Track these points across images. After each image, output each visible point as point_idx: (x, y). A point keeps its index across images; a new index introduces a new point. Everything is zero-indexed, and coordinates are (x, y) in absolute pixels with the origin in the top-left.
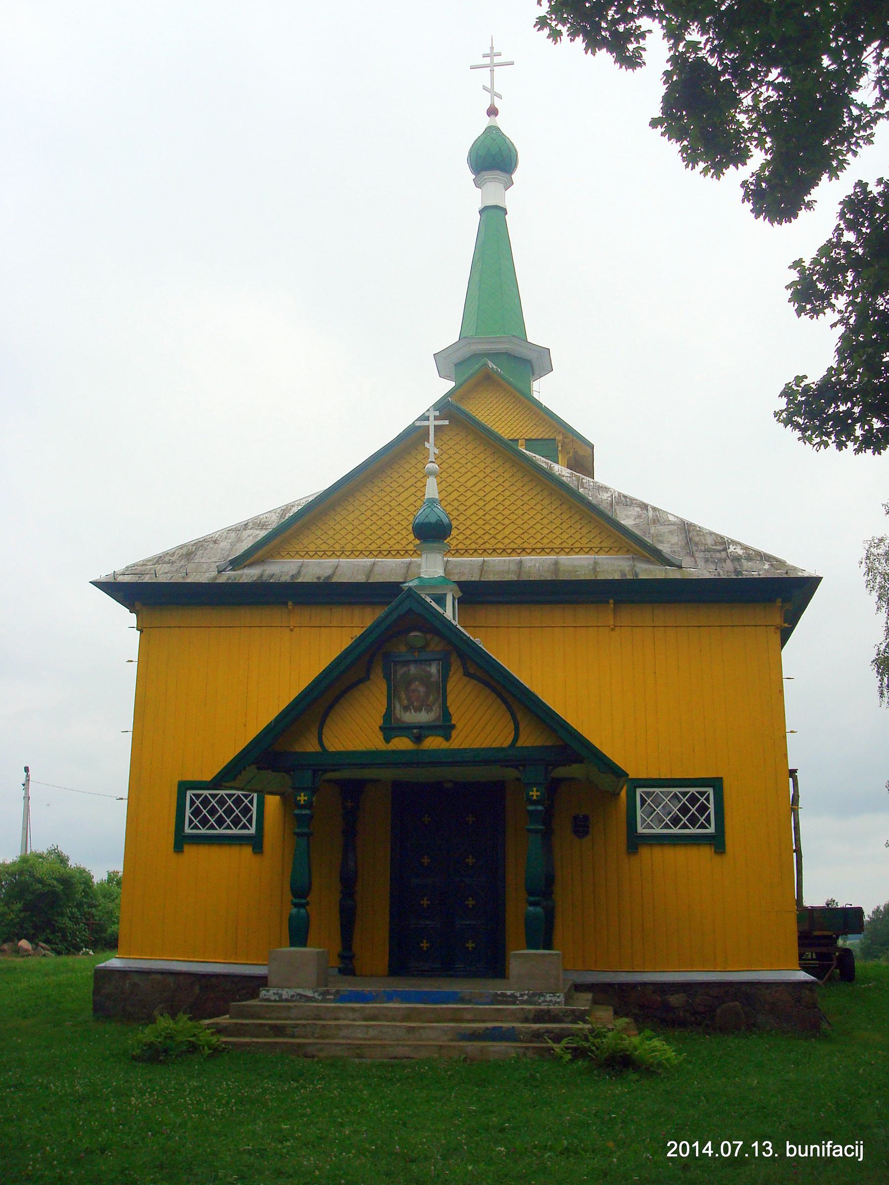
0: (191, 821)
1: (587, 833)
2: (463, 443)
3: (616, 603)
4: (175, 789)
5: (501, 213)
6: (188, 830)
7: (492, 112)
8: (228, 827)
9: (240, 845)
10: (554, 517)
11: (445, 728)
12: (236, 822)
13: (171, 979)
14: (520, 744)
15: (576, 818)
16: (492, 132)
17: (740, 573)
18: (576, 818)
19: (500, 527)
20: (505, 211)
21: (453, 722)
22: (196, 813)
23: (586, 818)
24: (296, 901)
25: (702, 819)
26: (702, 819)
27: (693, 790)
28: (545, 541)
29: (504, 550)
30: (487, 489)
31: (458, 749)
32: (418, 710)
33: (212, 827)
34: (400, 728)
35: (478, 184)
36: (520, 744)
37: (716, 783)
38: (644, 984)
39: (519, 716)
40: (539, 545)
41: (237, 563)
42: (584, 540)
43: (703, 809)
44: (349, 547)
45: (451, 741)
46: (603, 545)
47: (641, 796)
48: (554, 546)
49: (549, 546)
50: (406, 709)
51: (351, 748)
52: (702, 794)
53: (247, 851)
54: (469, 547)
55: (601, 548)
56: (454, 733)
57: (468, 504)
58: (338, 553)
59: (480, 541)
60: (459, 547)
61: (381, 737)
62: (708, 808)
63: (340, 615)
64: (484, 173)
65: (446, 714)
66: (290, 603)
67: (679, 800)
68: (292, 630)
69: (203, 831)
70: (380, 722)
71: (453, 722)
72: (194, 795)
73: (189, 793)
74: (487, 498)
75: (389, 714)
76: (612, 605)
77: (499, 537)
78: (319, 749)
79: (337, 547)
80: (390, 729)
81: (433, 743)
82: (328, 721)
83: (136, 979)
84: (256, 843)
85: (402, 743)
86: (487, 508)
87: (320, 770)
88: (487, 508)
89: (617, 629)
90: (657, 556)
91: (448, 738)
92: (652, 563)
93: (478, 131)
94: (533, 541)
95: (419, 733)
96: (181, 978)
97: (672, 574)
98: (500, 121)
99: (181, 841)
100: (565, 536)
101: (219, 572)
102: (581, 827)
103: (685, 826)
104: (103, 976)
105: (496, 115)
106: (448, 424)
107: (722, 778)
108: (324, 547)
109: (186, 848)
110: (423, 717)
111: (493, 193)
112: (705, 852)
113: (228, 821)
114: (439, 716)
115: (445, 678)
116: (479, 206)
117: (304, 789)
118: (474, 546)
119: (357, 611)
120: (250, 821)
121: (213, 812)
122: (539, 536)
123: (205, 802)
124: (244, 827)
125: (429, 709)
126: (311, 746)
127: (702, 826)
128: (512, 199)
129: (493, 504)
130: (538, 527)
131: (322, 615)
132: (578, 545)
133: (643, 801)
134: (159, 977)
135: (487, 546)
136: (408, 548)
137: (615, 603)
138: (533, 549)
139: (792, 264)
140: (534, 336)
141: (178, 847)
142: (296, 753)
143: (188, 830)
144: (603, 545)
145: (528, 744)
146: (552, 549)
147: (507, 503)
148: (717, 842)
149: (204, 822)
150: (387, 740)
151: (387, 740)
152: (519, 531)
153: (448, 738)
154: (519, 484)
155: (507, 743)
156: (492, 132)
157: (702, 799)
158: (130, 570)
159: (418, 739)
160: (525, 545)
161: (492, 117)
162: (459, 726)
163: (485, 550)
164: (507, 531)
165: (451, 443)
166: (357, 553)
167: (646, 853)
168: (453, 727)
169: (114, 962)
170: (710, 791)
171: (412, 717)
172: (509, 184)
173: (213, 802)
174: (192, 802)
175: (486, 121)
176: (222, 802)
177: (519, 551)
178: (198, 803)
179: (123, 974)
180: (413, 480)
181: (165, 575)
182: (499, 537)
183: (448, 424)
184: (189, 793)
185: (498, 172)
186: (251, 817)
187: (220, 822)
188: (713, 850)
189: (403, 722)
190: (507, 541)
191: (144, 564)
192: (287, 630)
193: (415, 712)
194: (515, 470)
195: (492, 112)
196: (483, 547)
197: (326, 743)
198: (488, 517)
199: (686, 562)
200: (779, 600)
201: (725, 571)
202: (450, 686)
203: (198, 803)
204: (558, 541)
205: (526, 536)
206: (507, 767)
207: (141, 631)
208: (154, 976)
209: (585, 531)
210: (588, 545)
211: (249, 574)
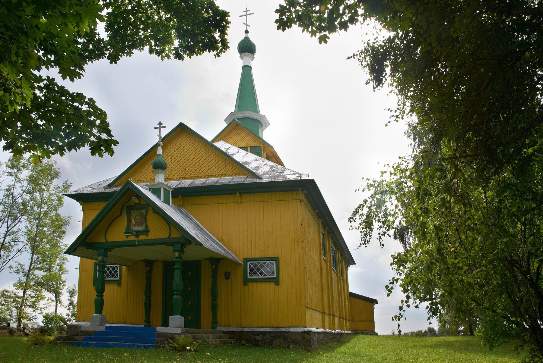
1: (229, 278)
2: (188, 138)
3: (240, 193)
9: (114, 283)
10: (219, 163)
11: (146, 232)
14: (172, 236)
15: (226, 273)
16: (247, 38)
18: (226, 273)
19: (200, 168)
23: (229, 273)
28: (216, 172)
30: (197, 154)
31: (151, 239)
32: (138, 226)
35: (241, 57)
36: (172, 236)
39: (172, 226)
41: (110, 186)
42: (231, 171)
44: (149, 179)
46: (237, 172)
47: (249, 264)
48: (220, 174)
49: (217, 174)
51: (115, 240)
53: (116, 285)
54: (190, 176)
55: (236, 174)
56: (149, 234)
57: (189, 160)
59: (193, 174)
60: (186, 176)
65: (147, 227)
71: (149, 229)
74: (196, 158)
75: (128, 227)
77: (200, 172)
80: (128, 232)
81: (142, 237)
82: (108, 231)
84: (119, 283)
85: (132, 238)
89: (242, 203)
91: (147, 236)
92: (254, 178)
93: (242, 38)
97: (257, 180)
102: (227, 276)
106: (93, 116)
110: (140, 228)
111: (247, 61)
112: (272, 285)
115: (147, 214)
118: (191, 176)
121: (110, 272)
124: (115, 277)
125: (142, 225)
126: (102, 240)
128: (254, 64)
133: (273, 273)
135: (196, 175)
136: (169, 178)
138: (212, 176)
142: (100, 243)
144: (237, 172)
145: (174, 236)
148: (276, 281)
150: (127, 237)
151: (127, 237)
153: (147, 236)
156: (247, 38)
159: (137, 236)
160: (209, 174)
161: (247, 33)
162: (151, 231)
163: (195, 177)
165: (182, 140)
167: (250, 285)
168: (149, 231)
172: (253, 59)
175: (244, 35)
177: (207, 177)
180: (171, 153)
182: (200, 172)
183: (93, 116)
190: (203, 173)
196: (194, 176)
204: (221, 172)
206: (169, 245)
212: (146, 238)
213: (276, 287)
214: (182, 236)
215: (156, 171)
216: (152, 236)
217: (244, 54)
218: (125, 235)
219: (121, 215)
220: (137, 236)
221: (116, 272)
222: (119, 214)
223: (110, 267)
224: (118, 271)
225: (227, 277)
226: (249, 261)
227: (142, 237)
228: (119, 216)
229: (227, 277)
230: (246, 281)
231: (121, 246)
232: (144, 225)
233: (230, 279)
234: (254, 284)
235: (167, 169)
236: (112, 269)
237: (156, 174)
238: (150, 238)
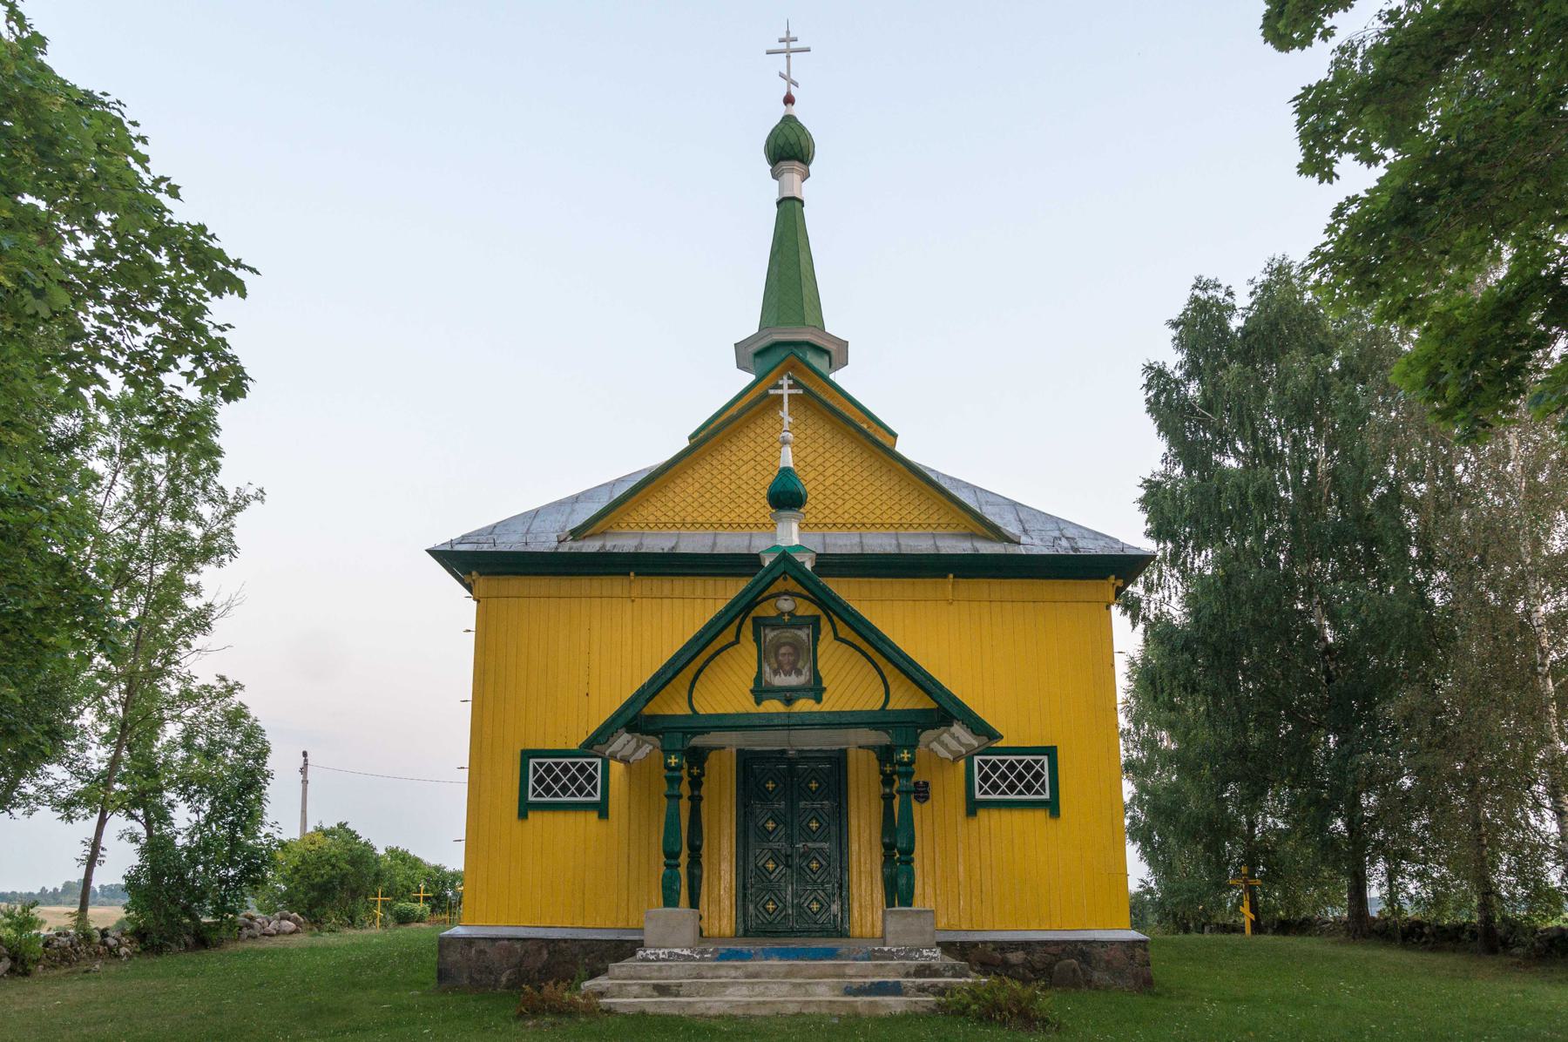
0: (534, 790)
1: (927, 798)
4: (518, 759)
5: (797, 204)
6: (531, 798)
7: (789, 100)
8: (573, 795)
11: (816, 689)
12: (580, 790)
13: (518, 946)
14: (889, 707)
16: (788, 120)
17: (1077, 550)
20: (802, 202)
21: (824, 685)
22: (540, 781)
23: (926, 784)
24: (669, 862)
25: (1037, 786)
26: (1037, 786)
27: (1028, 758)
28: (885, 516)
29: (844, 525)
32: (788, 673)
33: (556, 795)
34: (769, 691)
35: (775, 176)
36: (889, 707)
37: (1051, 752)
38: (985, 943)
40: (879, 521)
41: (577, 533)
43: (1038, 776)
44: (689, 519)
45: (822, 703)
46: (940, 521)
48: (893, 521)
50: (776, 672)
52: (1037, 762)
56: (825, 697)
58: (679, 526)
61: (753, 700)
62: (1043, 775)
63: (700, 585)
64: (782, 163)
65: (817, 677)
66: (632, 574)
67: (1016, 768)
68: (633, 601)
69: (547, 799)
70: (751, 686)
71: (824, 685)
72: (537, 763)
73: (532, 762)
75: (759, 678)
76: (951, 580)
77: (840, 511)
78: (690, 712)
79: (677, 519)
80: (761, 691)
81: (804, 705)
83: (482, 945)
84: (602, 809)
85: (773, 706)
86: (827, 484)
87: (689, 733)
88: (827, 484)
90: (996, 533)
91: (819, 700)
94: (872, 516)
95: (789, 695)
96: (529, 943)
97: (1012, 550)
98: (795, 110)
99: (525, 809)
100: (904, 512)
101: (560, 542)
103: (1020, 793)
104: (445, 944)
105: (793, 104)
107: (1056, 747)
108: (663, 519)
109: (530, 815)
110: (793, 680)
112: (1041, 815)
113: (573, 789)
114: (810, 679)
116: (776, 197)
117: (674, 751)
119: (720, 581)
120: (594, 788)
121: (556, 779)
122: (878, 512)
123: (549, 770)
124: (589, 794)
125: (799, 673)
126: (681, 709)
127: (1037, 792)
128: (809, 191)
129: (832, 479)
130: (878, 503)
131: (681, 585)
132: (916, 521)
134: (506, 942)
135: (827, 520)
136: (748, 521)
137: (955, 577)
139: (1377, 184)
140: (835, 324)
141: (523, 815)
143: (531, 798)
145: (899, 707)
146: (892, 525)
147: (846, 478)
149: (548, 790)
150: (758, 703)
151: (758, 703)
152: (858, 507)
153: (819, 700)
154: (858, 460)
155: (877, 708)
156: (788, 120)
157: (1037, 767)
158: (464, 539)
159: (789, 702)
161: (790, 105)
164: (847, 506)
166: (697, 526)
167: (982, 814)
169: (459, 931)
170: (1045, 759)
171: (780, 681)
172: (806, 176)
173: (557, 770)
174: (536, 771)
175: (781, 111)
176: (566, 770)
178: (541, 771)
179: (469, 942)
181: (511, 543)
184: (532, 762)
185: (797, 163)
186: (596, 784)
187: (564, 789)
188: (1048, 814)
189: (773, 686)
191: (479, 533)
192: (629, 600)
193: (785, 675)
194: (854, 446)
195: (789, 100)
196: (823, 521)
197: (696, 707)
198: (828, 492)
199: (1024, 539)
200: (1113, 577)
201: (1064, 548)
202: (820, 650)
203: (541, 771)
204: (897, 517)
205: (865, 512)
207: (478, 601)
208: (501, 942)
209: (923, 507)
210: (927, 521)
211: (591, 546)
212: (817, 708)
213: (1051, 822)
214: (933, 705)
215: (784, 513)
216: (830, 703)
217: (785, 165)
218: (751, 698)
219: (737, 641)
220: (789, 702)
221: (591, 778)
222: (733, 639)
223: (556, 764)
224: (599, 777)
225: (921, 795)
226: (978, 754)
227: (804, 705)
228: (732, 644)
229: (921, 795)
230: (973, 807)
231: (741, 727)
232: (806, 671)
233: (929, 802)
234: (995, 814)
235: (808, 506)
236: (577, 770)
237: (778, 519)
238: (828, 710)
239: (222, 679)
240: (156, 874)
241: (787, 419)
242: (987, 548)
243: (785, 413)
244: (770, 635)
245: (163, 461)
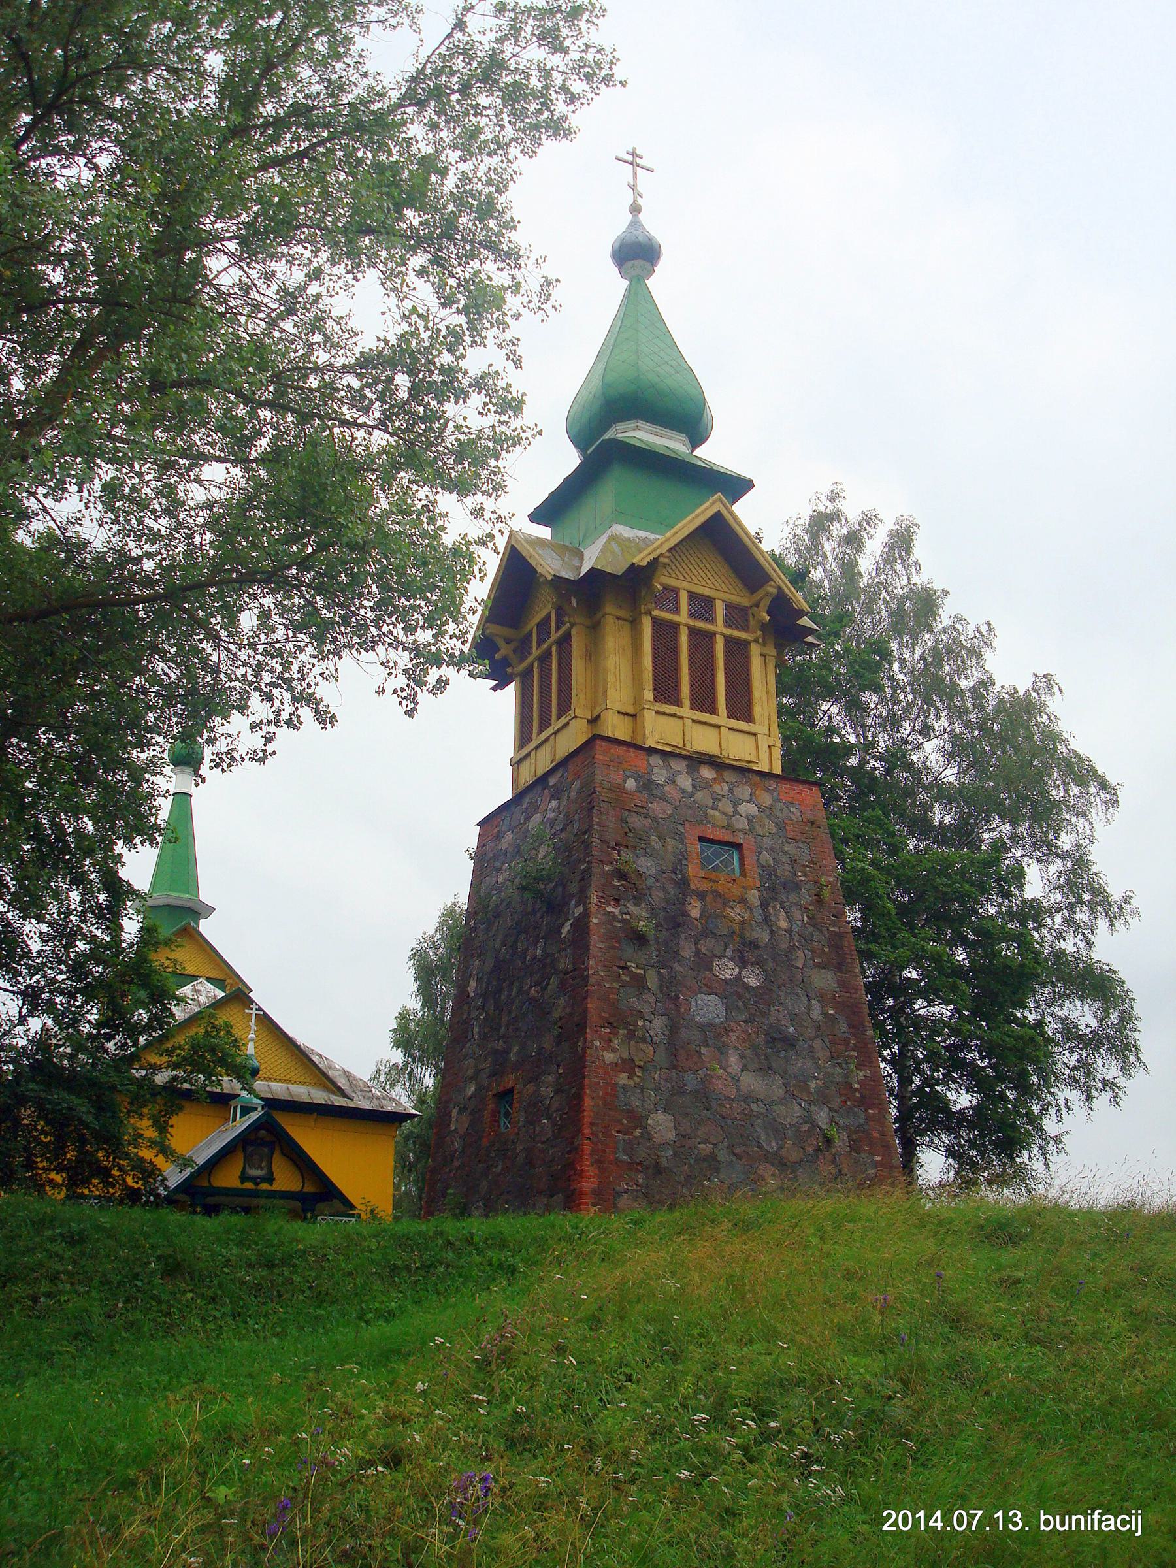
11: (270, 1179)
32: (257, 1169)
80: (244, 1178)
81: (264, 1186)
85: (249, 1185)
90: (342, 1093)
91: (271, 1184)
95: (256, 1180)
125: (262, 1169)
126: (206, 1184)
153: (271, 1184)
159: (257, 1184)
216: (276, 1187)
227: (264, 1186)
239: (274, 753)
240: (141, 816)
241: (254, 1027)
242: (339, 1101)
243: (252, 1023)
244: (250, 1149)
245: (382, 1404)
